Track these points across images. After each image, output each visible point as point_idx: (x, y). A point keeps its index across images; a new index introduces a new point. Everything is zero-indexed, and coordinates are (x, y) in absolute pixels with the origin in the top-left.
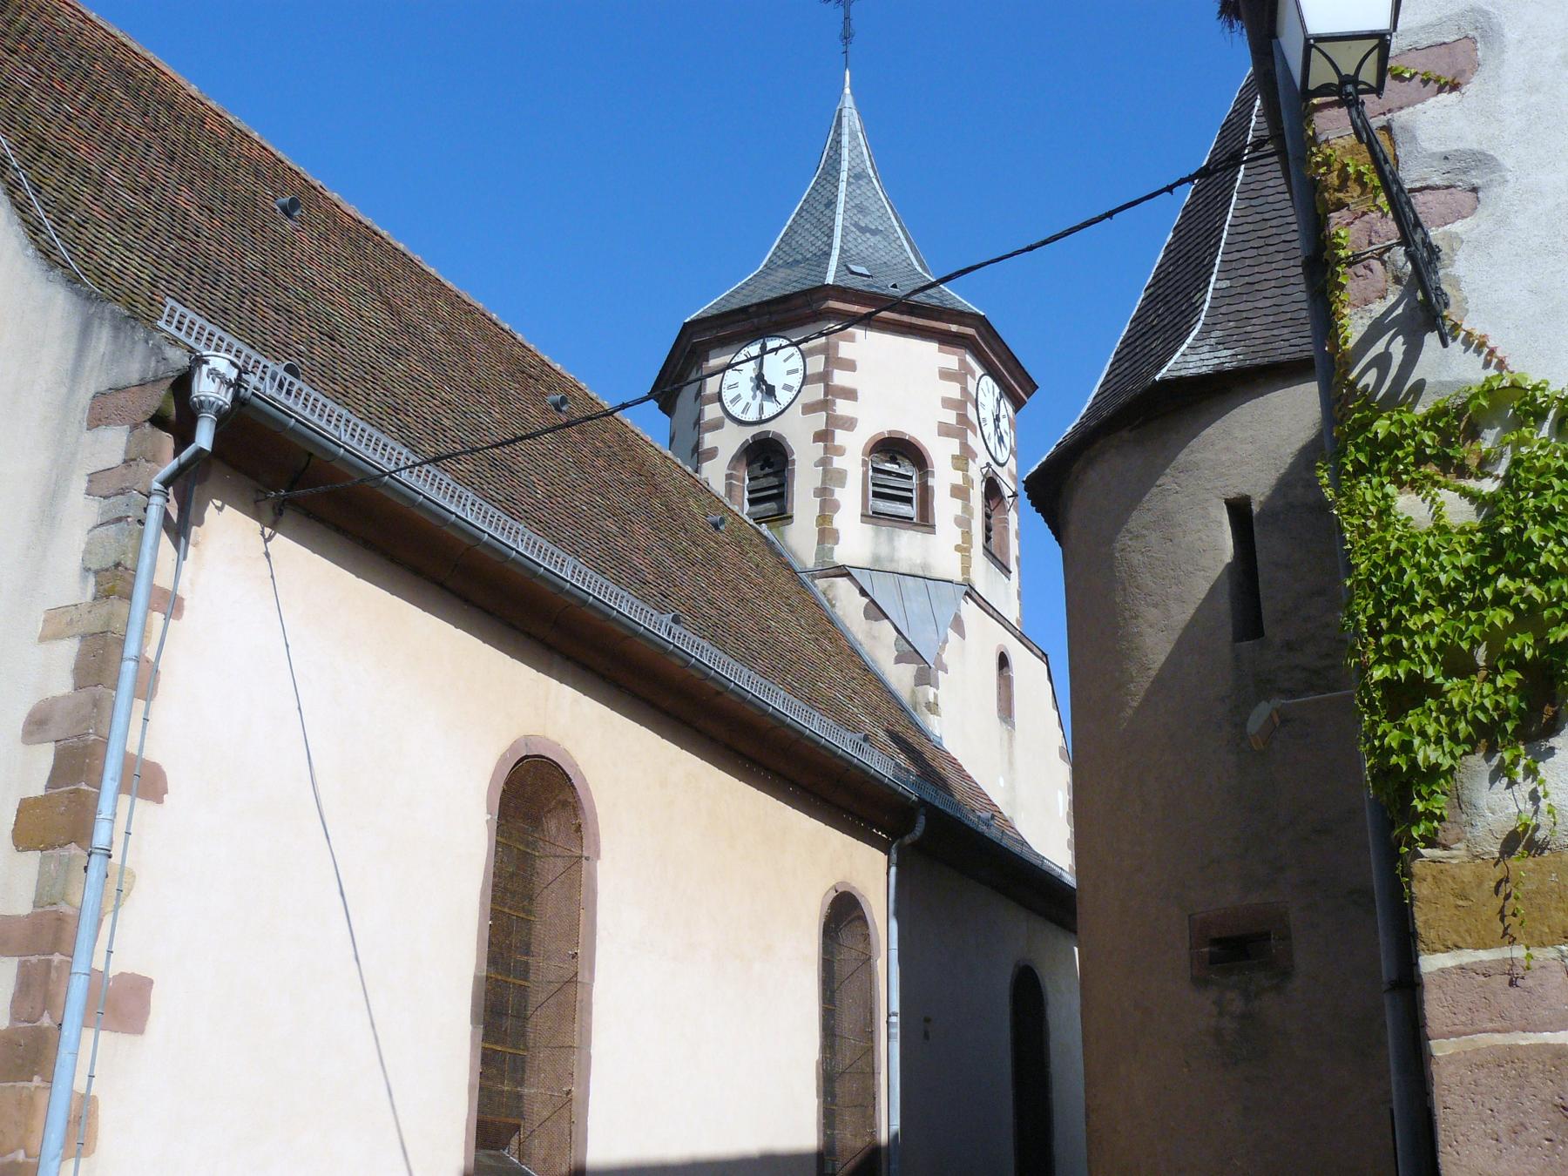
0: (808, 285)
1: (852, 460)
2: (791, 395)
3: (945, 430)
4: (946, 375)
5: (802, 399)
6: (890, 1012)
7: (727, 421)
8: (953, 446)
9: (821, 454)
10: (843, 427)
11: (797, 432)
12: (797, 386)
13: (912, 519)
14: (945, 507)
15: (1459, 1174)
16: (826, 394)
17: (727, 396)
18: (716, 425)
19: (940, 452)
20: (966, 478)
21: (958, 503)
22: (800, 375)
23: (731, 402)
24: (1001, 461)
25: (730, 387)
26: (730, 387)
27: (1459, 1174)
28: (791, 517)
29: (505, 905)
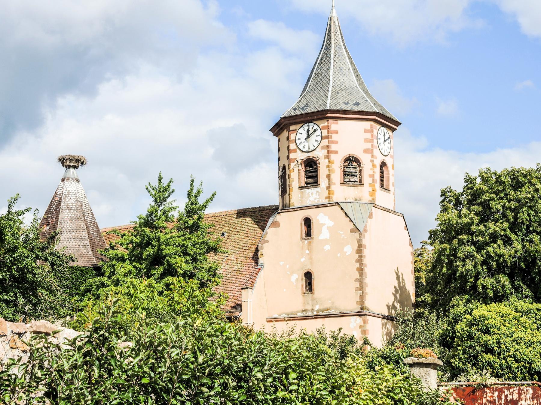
0: (322, 108)
1: (338, 160)
2: (318, 143)
3: (366, 151)
4: (366, 131)
5: (321, 145)
6: (326, 201)
7: (298, 150)
8: (369, 156)
9: (327, 164)
10: (333, 143)
11: (319, 154)
12: (319, 140)
13: (357, 182)
14: (366, 180)
15: (254, 403)
16: (328, 133)
17: (298, 142)
18: (295, 151)
19: (365, 159)
20: (373, 180)
21: (371, 179)
22: (320, 137)
23: (299, 144)
24: (386, 154)
25: (299, 139)
26: (299, 139)
27: (254, 403)
28: (319, 185)
29: (54, 232)
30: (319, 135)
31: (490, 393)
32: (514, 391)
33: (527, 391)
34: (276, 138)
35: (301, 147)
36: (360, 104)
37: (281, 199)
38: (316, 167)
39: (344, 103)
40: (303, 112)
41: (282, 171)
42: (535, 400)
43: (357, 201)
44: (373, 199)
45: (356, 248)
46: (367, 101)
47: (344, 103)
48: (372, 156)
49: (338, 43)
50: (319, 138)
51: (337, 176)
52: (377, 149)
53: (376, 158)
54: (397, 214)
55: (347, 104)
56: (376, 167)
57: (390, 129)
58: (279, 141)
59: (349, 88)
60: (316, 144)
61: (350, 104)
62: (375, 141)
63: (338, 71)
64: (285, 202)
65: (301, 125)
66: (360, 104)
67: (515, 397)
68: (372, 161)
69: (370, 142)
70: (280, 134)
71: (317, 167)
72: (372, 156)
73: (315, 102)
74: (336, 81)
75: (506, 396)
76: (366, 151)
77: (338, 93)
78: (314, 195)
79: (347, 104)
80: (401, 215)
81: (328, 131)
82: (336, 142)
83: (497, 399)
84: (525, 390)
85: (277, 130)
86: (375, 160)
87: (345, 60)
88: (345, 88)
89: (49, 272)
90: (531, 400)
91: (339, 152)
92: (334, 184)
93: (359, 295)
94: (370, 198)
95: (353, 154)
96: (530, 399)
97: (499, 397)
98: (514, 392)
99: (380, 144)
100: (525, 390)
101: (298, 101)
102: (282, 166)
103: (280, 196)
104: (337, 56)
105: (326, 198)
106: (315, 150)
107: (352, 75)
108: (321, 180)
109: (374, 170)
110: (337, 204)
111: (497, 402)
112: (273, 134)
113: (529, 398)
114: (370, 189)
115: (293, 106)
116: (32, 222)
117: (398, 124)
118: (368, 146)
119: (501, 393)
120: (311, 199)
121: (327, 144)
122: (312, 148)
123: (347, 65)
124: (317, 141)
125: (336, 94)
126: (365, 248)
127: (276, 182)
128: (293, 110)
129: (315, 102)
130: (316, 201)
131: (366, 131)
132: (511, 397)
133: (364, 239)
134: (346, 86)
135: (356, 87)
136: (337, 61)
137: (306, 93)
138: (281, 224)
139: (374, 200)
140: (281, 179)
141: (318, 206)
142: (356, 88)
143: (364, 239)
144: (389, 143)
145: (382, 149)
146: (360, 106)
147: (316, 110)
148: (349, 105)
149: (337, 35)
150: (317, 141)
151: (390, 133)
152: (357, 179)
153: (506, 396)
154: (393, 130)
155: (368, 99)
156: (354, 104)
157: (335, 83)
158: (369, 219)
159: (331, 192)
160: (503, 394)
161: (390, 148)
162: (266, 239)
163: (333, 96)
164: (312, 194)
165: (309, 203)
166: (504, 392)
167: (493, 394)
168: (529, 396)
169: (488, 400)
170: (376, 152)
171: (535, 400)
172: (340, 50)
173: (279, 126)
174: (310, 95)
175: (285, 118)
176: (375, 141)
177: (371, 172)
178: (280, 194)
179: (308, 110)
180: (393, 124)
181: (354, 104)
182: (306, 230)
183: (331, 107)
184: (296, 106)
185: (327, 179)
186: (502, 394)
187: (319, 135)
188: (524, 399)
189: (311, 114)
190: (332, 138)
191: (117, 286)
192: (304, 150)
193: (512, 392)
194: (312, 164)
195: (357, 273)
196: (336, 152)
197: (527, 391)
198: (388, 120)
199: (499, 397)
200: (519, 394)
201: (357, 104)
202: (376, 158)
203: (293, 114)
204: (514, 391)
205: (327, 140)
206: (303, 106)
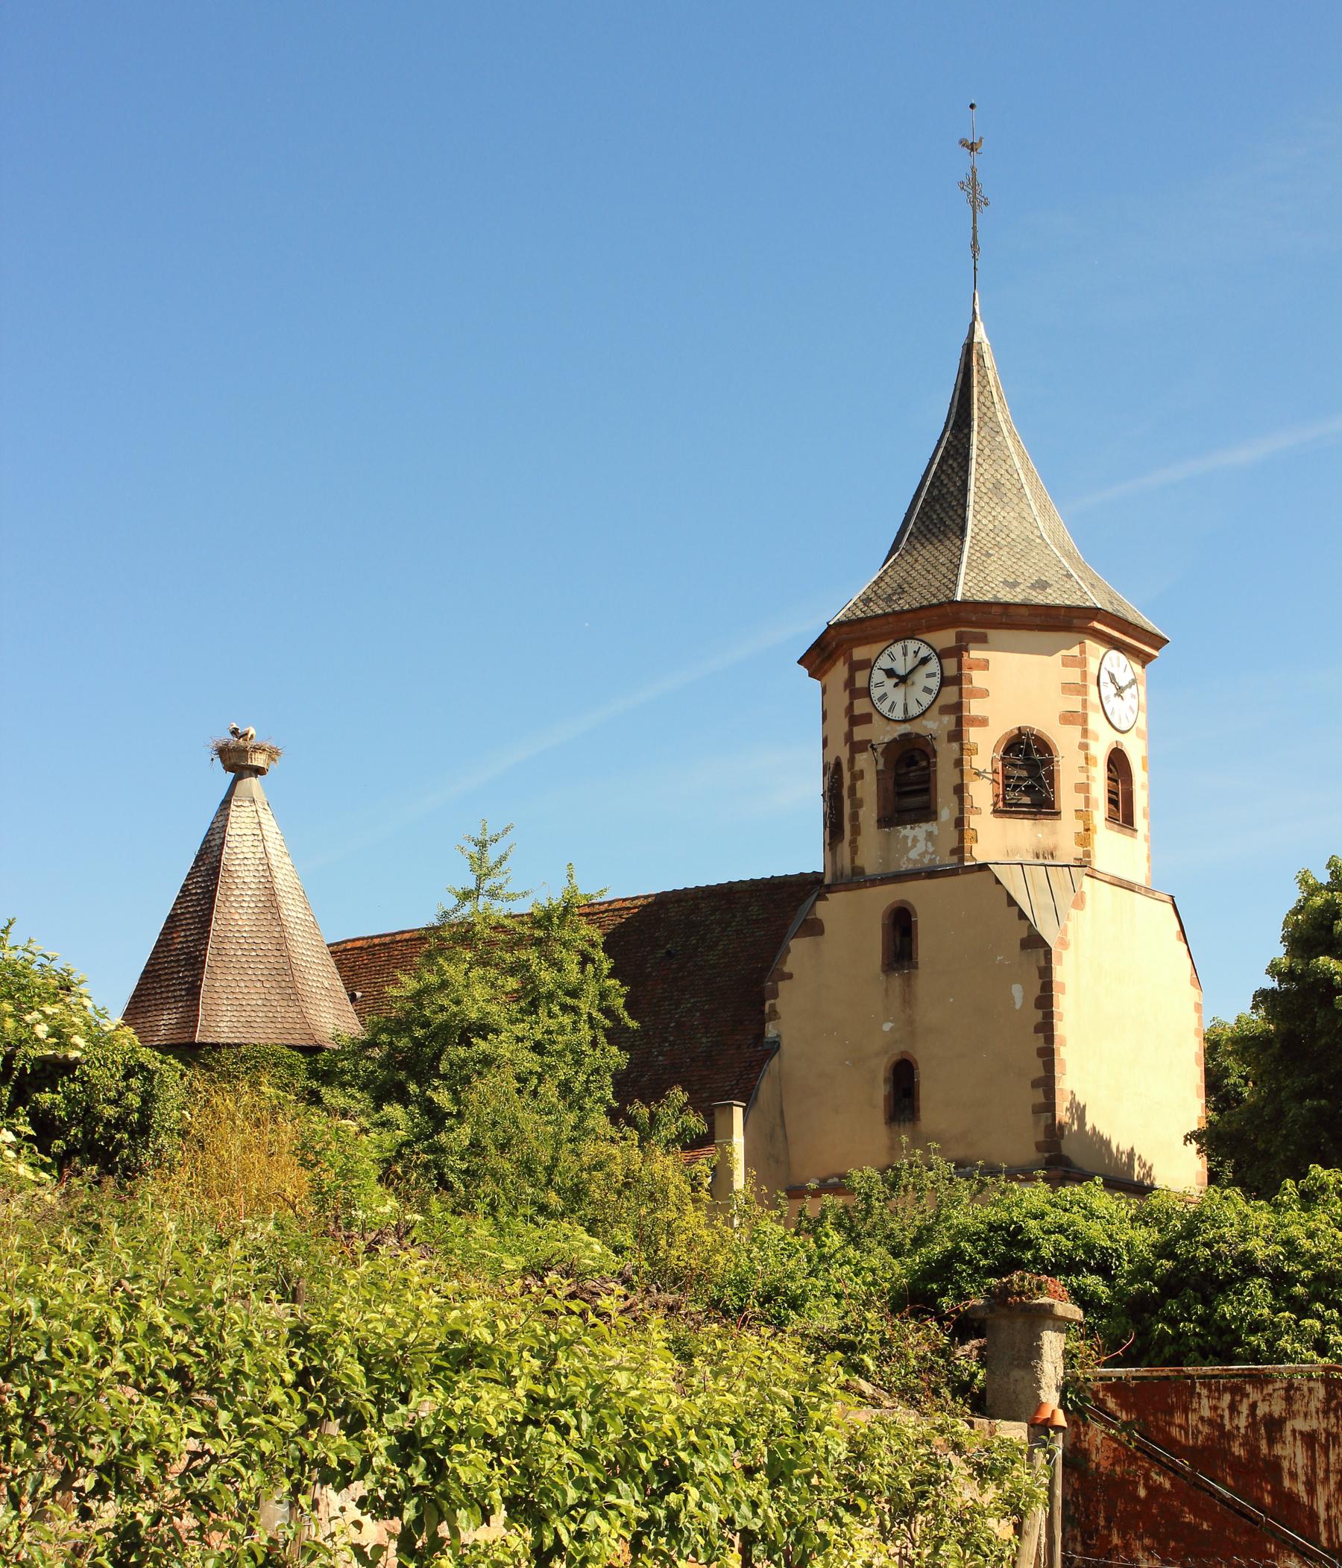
3: (1068, 718)
5: (941, 702)
14: (1067, 798)
19: (1064, 741)
23: (879, 699)
25: (877, 685)
26: (877, 685)
30: (933, 675)
31: (1208, 1397)
32: (1274, 1390)
33: (1310, 1390)
34: (816, 685)
35: (884, 708)
36: (1051, 586)
37: (828, 853)
38: (924, 763)
39: (1005, 582)
40: (889, 610)
41: (832, 777)
42: (1332, 1415)
43: (1041, 861)
44: (1087, 854)
45: (1037, 991)
46: (1069, 576)
47: (1005, 582)
49: (989, 414)
50: (934, 683)
51: (982, 793)
53: (1096, 739)
54: (1157, 895)
55: (1014, 585)
56: (1095, 764)
57: (1138, 657)
58: (824, 691)
59: (1019, 540)
60: (926, 699)
61: (1022, 587)
62: (1093, 689)
63: (990, 495)
64: (839, 866)
65: (885, 644)
66: (1051, 586)
67: (1278, 1408)
68: (1084, 747)
69: (1079, 693)
70: (825, 673)
71: (929, 762)
73: (922, 581)
74: (984, 521)
75: (1253, 1407)
76: (1068, 718)
77: (989, 555)
78: (921, 847)
79: (1014, 585)
80: (1168, 899)
82: (984, 694)
83: (1227, 1413)
84: (1305, 1389)
85: (817, 662)
86: (1092, 743)
87: (1009, 462)
88: (1008, 539)
89: (573, 916)
90: (1321, 1415)
91: (990, 721)
93: (1042, 1124)
94: (1079, 852)
95: (1030, 728)
96: (1317, 1413)
97: (1233, 1408)
98: (1275, 1395)
99: (1108, 697)
100: (1305, 1389)
101: (875, 578)
102: (833, 762)
103: (827, 847)
104: (987, 452)
105: (953, 852)
106: (923, 713)
107: (1029, 505)
108: (939, 800)
110: (984, 867)
111: (1227, 1422)
112: (806, 671)
113: (1314, 1410)
114: (1080, 827)
115: (861, 593)
117: (1158, 642)
118: (1074, 704)
119: (1238, 1398)
120: (913, 854)
121: (955, 699)
122: (914, 710)
123: (1016, 476)
124: (927, 690)
125: (983, 558)
126: (1063, 993)
127: (817, 808)
128: (861, 605)
129: (922, 581)
130: (926, 861)
132: (1267, 1409)
133: (1058, 967)
134: (1012, 536)
135: (1041, 537)
136: (985, 466)
137: (900, 555)
138: (828, 927)
139: (1089, 856)
140: (830, 797)
141: (931, 873)
142: (1038, 541)
143: (1058, 967)
144: (1133, 696)
145: (1113, 713)
146: (1048, 590)
147: (925, 603)
148: (1018, 590)
149: (986, 393)
150: (927, 690)
151: (1138, 668)
153: (1253, 1407)
154: (1145, 659)
155: (1072, 572)
156: (1033, 587)
157: (980, 526)
158: (1073, 912)
159: (968, 834)
160: (1245, 1400)
161: (1135, 708)
162: (786, 969)
163: (974, 564)
164: (915, 840)
165: (905, 866)
166: (1248, 1395)
167: (1219, 1399)
168: (1314, 1404)
169: (1202, 1418)
170: (1096, 721)
171: (1332, 1415)
172: (993, 434)
173: (823, 650)
174: (910, 560)
175: (839, 624)
176: (1093, 689)
177: (1082, 778)
178: (828, 841)
179: (903, 604)
180: (1145, 643)
181: (1033, 587)
182: (898, 943)
183: (969, 594)
184: (869, 592)
185: (955, 799)
186: (1241, 1401)
187: (933, 675)
188: (1302, 1415)
189: (911, 615)
192: (892, 716)
193: (1270, 1395)
194: (913, 756)
195: (1039, 1062)
196: (983, 722)
197: (1310, 1390)
198: (1131, 631)
199: (1233, 1408)
200: (1289, 1399)
201: (1042, 585)
202: (1096, 739)
203: (862, 615)
204: (1274, 1390)
205: (955, 688)
206: (890, 591)
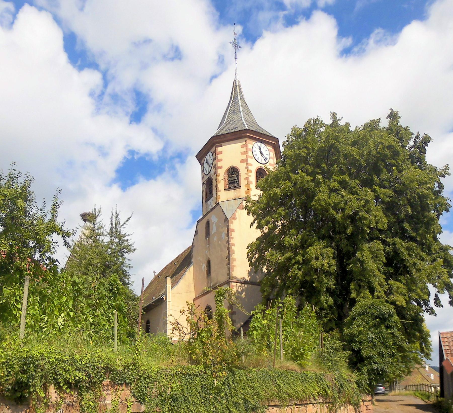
3: (242, 161)
8: (244, 165)
14: (243, 182)
48: (247, 164)
52: (252, 158)
53: (251, 165)
68: (247, 168)
72: (247, 164)
76: (242, 161)
81: (247, 156)
92: (220, 191)
109: (248, 174)
114: (246, 189)
116: (58, 244)
118: (244, 157)
131: (242, 147)
152: (236, 185)
178: (204, 200)
180: (270, 140)
190: (218, 158)
191: (365, 186)
196: (221, 167)
